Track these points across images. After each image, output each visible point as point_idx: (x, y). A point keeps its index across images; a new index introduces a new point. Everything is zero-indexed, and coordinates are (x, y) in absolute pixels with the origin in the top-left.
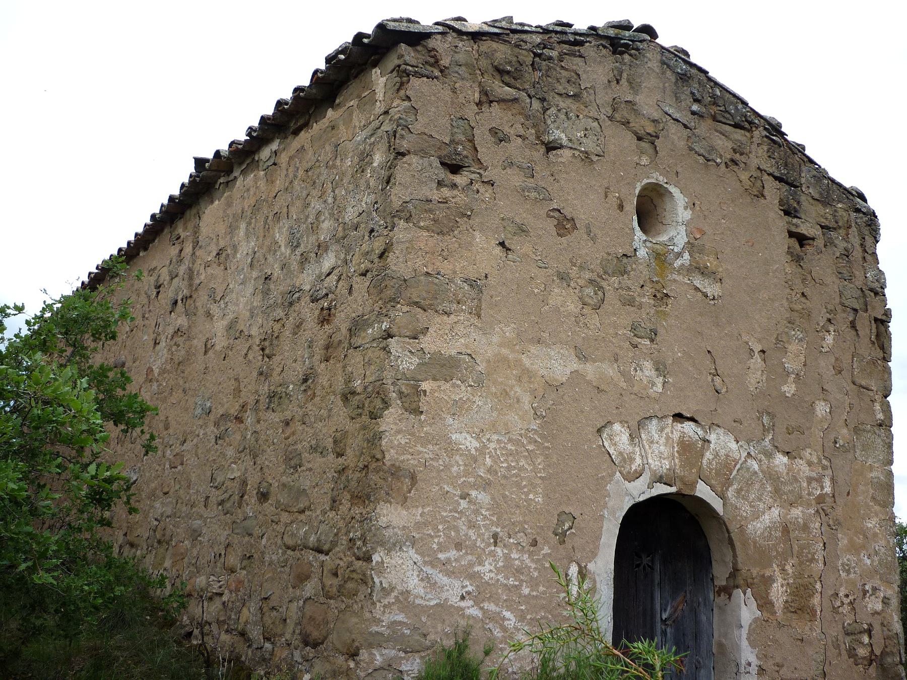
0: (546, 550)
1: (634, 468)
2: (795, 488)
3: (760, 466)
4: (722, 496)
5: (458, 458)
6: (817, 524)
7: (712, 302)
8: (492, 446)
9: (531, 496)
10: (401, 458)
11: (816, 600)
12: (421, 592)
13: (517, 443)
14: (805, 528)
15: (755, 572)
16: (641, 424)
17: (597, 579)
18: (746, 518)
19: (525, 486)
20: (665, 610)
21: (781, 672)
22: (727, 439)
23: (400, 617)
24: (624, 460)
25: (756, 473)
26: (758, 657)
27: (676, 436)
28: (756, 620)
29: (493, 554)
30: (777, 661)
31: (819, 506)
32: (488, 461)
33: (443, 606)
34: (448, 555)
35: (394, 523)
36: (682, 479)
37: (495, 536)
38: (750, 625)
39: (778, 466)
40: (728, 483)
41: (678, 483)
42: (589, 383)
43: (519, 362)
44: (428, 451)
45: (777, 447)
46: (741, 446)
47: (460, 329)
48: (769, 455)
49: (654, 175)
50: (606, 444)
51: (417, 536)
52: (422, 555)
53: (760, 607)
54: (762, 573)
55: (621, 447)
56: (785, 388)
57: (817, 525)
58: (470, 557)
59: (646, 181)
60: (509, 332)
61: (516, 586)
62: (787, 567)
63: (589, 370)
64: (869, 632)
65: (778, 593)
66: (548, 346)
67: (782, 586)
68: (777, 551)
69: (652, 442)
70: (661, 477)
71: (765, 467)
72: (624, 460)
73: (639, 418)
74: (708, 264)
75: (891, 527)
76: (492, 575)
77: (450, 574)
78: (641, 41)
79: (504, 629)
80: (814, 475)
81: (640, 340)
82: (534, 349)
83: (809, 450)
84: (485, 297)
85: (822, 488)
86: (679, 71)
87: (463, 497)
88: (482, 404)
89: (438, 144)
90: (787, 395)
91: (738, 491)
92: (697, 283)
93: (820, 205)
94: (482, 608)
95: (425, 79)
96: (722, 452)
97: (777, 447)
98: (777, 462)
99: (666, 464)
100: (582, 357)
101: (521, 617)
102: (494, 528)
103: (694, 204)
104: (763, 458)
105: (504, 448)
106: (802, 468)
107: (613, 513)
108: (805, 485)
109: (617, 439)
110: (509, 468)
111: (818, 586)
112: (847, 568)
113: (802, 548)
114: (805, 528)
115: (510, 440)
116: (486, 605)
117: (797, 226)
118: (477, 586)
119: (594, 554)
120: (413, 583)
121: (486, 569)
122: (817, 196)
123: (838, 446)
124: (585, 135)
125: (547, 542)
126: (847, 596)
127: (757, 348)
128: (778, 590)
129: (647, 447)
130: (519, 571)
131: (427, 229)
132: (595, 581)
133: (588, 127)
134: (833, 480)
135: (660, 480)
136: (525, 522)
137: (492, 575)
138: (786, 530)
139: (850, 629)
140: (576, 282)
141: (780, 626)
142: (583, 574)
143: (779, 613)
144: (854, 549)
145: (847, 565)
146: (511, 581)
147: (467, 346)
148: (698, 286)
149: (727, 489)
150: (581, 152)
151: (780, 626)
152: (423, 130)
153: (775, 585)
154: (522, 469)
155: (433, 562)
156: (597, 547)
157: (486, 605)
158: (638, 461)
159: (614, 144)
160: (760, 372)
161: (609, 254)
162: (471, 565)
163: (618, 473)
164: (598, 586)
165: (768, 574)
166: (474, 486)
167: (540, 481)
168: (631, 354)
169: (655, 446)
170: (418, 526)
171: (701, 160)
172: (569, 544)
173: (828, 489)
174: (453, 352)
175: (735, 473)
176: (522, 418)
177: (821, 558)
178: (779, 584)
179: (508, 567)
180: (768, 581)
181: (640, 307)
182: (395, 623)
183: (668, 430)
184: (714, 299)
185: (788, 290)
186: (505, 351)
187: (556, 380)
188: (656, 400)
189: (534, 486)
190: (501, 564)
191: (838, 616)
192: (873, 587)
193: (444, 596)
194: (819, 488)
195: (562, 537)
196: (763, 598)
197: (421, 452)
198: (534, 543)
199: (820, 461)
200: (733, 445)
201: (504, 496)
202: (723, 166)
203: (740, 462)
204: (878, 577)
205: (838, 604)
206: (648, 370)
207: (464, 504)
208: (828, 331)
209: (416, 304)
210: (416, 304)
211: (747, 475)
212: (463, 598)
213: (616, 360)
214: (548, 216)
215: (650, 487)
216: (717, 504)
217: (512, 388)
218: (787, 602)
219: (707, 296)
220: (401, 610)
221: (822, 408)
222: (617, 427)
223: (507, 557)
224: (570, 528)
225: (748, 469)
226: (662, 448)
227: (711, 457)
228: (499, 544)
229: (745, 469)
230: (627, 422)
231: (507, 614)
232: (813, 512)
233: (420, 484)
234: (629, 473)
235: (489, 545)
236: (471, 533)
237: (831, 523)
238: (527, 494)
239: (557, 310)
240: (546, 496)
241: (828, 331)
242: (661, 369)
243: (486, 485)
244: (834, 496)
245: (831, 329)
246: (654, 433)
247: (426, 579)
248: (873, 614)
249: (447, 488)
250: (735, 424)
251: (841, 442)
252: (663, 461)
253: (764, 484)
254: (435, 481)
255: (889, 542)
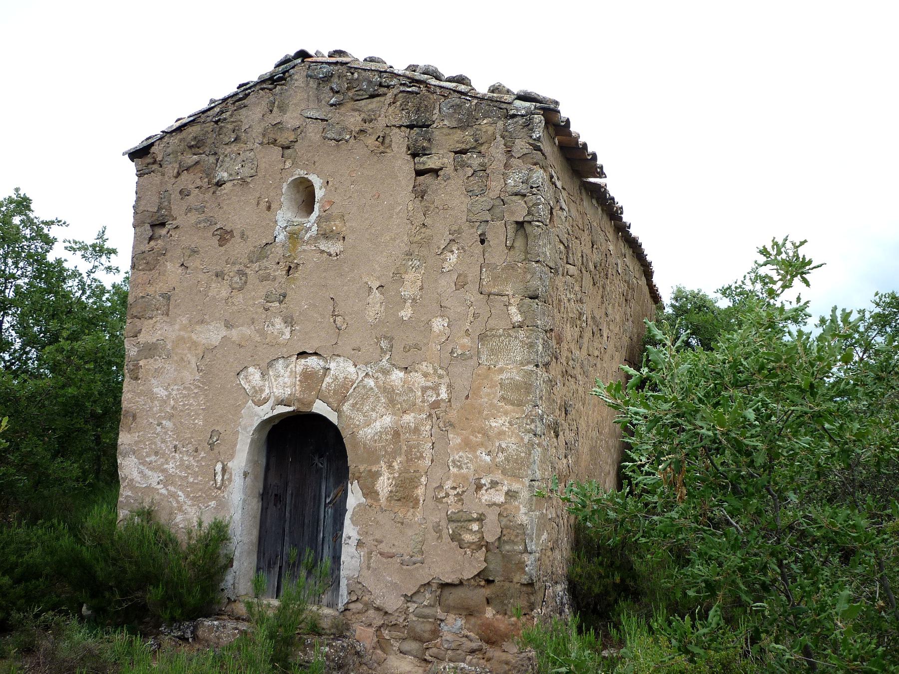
0: (203, 454)
1: (263, 396)
2: (410, 397)
3: (376, 383)
4: (337, 410)
5: (156, 402)
6: (428, 427)
7: (336, 258)
8: (174, 393)
9: (196, 421)
10: (129, 406)
11: (420, 491)
12: (139, 479)
13: (189, 389)
14: (416, 430)
15: (362, 468)
16: (270, 365)
17: (233, 473)
18: (358, 425)
19: (193, 416)
20: (329, 497)
21: (378, 547)
22: (346, 364)
23: (129, 493)
24: (256, 392)
25: (372, 389)
26: (358, 533)
27: (299, 369)
28: (359, 505)
29: (173, 457)
30: (376, 537)
31: (433, 412)
32: (172, 402)
33: (148, 487)
34: (150, 459)
35: (125, 443)
36: (299, 400)
37: (175, 447)
38: (355, 508)
39: (394, 381)
40: (345, 399)
41: (296, 404)
42: (234, 342)
43: (190, 337)
44: (141, 400)
45: (394, 365)
46: (360, 369)
47: (158, 326)
48: (386, 372)
49: (297, 172)
50: (242, 382)
51: (136, 449)
52: (139, 459)
53: (365, 495)
54: (369, 469)
55: (254, 383)
56: (402, 313)
57: (428, 427)
58: (162, 460)
59: (291, 179)
60: (185, 321)
61: (185, 477)
62: (395, 464)
63: (234, 334)
64: (480, 519)
65: (384, 485)
66: (208, 323)
67: (389, 479)
68: (386, 451)
69: (279, 376)
70: (282, 401)
71: (381, 383)
72: (256, 392)
73: (269, 361)
74: (334, 228)
75: (527, 424)
76: (174, 470)
77: (152, 469)
78: (293, 67)
79: (178, 502)
80: (430, 384)
81: (270, 304)
82: (198, 328)
83: (425, 364)
84: (172, 302)
85: (438, 395)
86: (321, 76)
87: (159, 424)
88: (170, 368)
89: (151, 214)
90: (404, 319)
91: (353, 405)
92: (322, 248)
93: (459, 132)
94: (167, 489)
95: (146, 176)
96: (341, 376)
97: (394, 365)
98: (393, 377)
99: (288, 391)
100: (228, 325)
101: (187, 496)
102: (175, 442)
103: (328, 182)
104: (381, 375)
105: (181, 393)
106: (418, 379)
107: (245, 429)
108: (420, 394)
109: (251, 378)
110: (184, 405)
111: (423, 480)
112: (459, 464)
113: (410, 448)
114: (416, 430)
115: (185, 388)
116: (169, 488)
117: (424, 164)
118: (165, 477)
119: (232, 456)
120: (136, 475)
121: (170, 467)
122: (454, 124)
123: (455, 355)
124: (242, 166)
125: (203, 449)
126: (454, 488)
127: (375, 284)
128: (383, 482)
129: (273, 381)
130: (188, 467)
131: (143, 270)
132: (231, 474)
133: (245, 159)
134: (450, 386)
135: (281, 402)
136: (192, 438)
137: (174, 470)
138: (397, 434)
139: (455, 517)
140: (229, 275)
141: (383, 510)
142: (224, 470)
143: (383, 500)
144: (467, 445)
145: (459, 461)
146: (183, 474)
147: (161, 335)
148: (323, 248)
149: (343, 405)
150: (239, 179)
151: (383, 510)
152: (143, 209)
153: (382, 478)
154: (191, 405)
155: (144, 464)
156: (234, 452)
157: (169, 488)
158: (267, 391)
159: (265, 162)
160: (379, 305)
161: (255, 247)
162: (162, 464)
163: (250, 401)
164: (233, 477)
165: (374, 469)
166: (164, 418)
167: (202, 411)
168: (264, 316)
169: (280, 379)
170: (137, 443)
171: (333, 143)
172: (216, 451)
173: (444, 395)
174: (154, 340)
175: (351, 390)
176: (191, 373)
177: (429, 455)
178: (386, 477)
179: (182, 466)
180: (376, 475)
181: (275, 279)
182: (127, 496)
183: (292, 366)
184: (337, 255)
185: (410, 226)
186: (182, 333)
187: (212, 345)
188: (285, 345)
189: (198, 415)
190: (178, 463)
191: (442, 505)
192: (492, 481)
193: (150, 482)
194: (435, 396)
195: (212, 446)
196: (368, 488)
197: (138, 401)
198: (196, 451)
199: (435, 370)
200: (352, 369)
201: (181, 423)
202: (352, 141)
203: (357, 382)
204: (500, 471)
205: (442, 494)
206: (278, 323)
207: (159, 429)
208: (452, 251)
209: (136, 316)
210: (136, 316)
211: (363, 392)
212: (158, 483)
213: (253, 323)
214: (213, 235)
215: (273, 409)
216: (333, 417)
217: (185, 355)
218: (391, 492)
219: (330, 255)
220: (130, 489)
221: (439, 324)
222: (251, 370)
223: (182, 460)
224: (217, 440)
225: (364, 387)
226: (286, 380)
227: (331, 381)
228: (178, 452)
229: (361, 387)
230: (258, 365)
231: (180, 493)
232: (425, 416)
233: (138, 420)
234: (259, 400)
235: (172, 452)
236: (163, 445)
237: (441, 425)
238: (194, 420)
239: (214, 298)
240: (205, 420)
241: (452, 251)
242: (289, 321)
243: (171, 417)
244: (450, 401)
245: (454, 248)
246: (280, 369)
247: (141, 472)
248: (489, 506)
249: (151, 420)
250: (353, 352)
251: (459, 352)
252: (286, 389)
253: (379, 397)
254: (145, 417)
255: (522, 439)
